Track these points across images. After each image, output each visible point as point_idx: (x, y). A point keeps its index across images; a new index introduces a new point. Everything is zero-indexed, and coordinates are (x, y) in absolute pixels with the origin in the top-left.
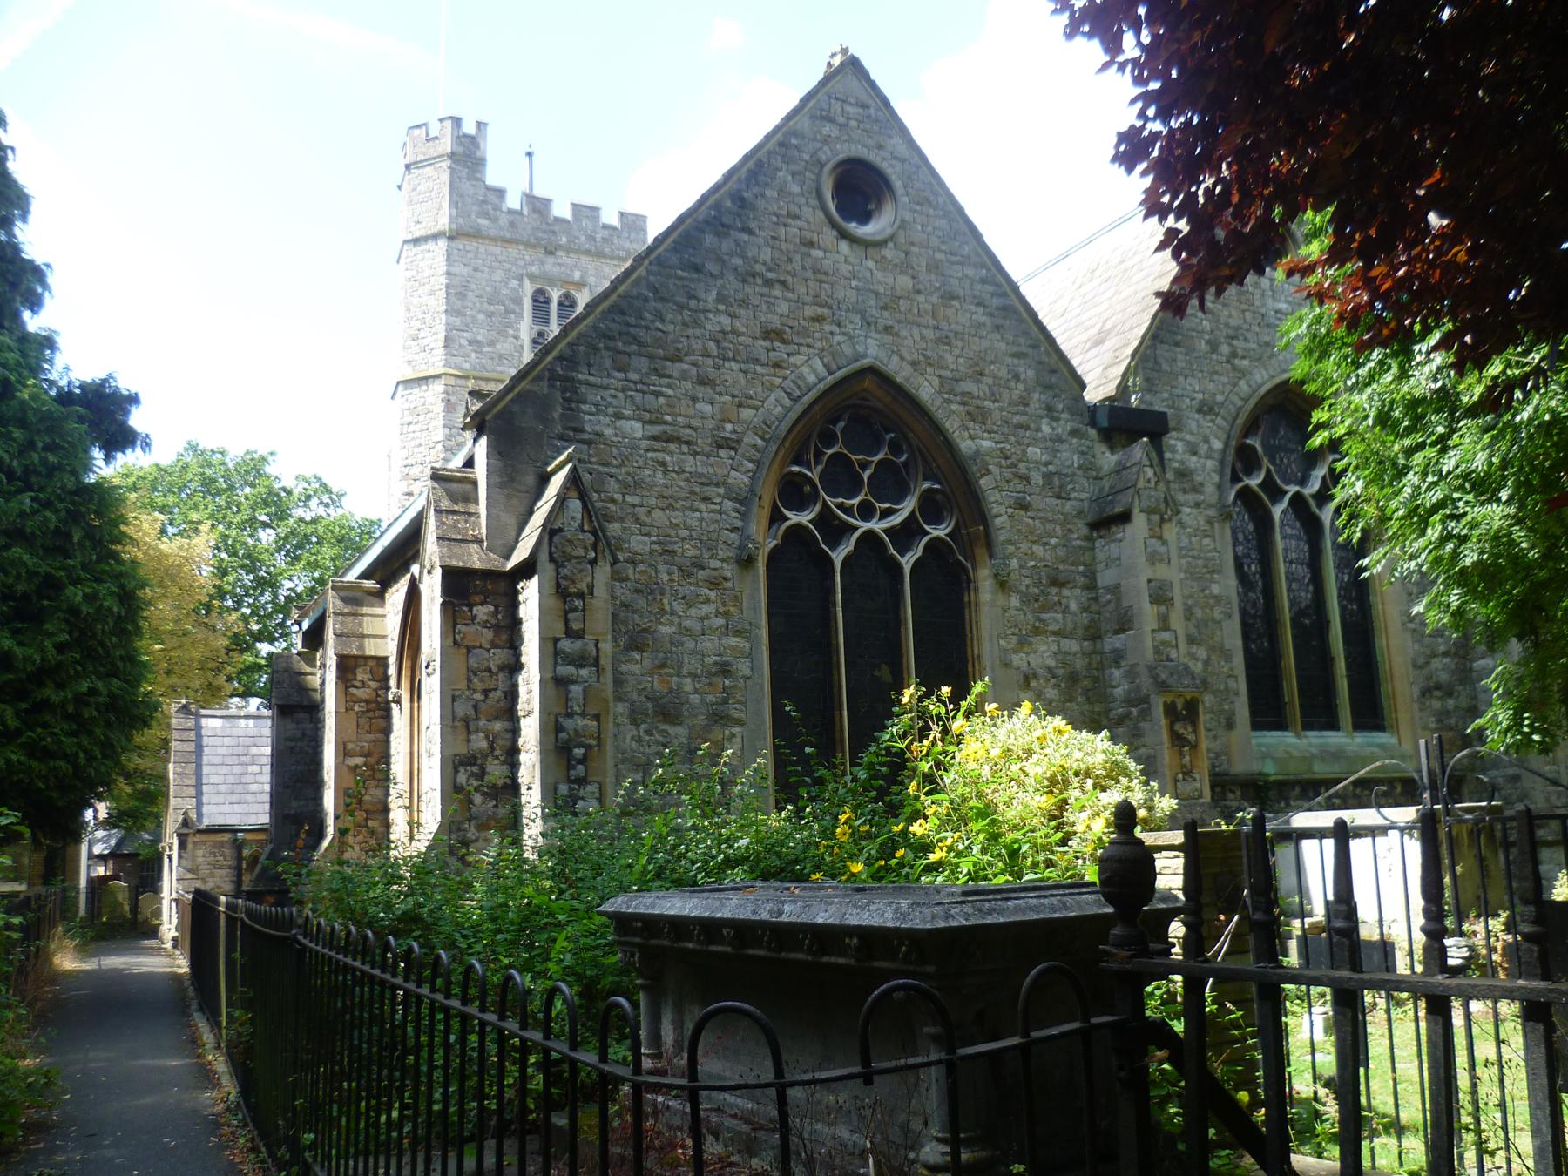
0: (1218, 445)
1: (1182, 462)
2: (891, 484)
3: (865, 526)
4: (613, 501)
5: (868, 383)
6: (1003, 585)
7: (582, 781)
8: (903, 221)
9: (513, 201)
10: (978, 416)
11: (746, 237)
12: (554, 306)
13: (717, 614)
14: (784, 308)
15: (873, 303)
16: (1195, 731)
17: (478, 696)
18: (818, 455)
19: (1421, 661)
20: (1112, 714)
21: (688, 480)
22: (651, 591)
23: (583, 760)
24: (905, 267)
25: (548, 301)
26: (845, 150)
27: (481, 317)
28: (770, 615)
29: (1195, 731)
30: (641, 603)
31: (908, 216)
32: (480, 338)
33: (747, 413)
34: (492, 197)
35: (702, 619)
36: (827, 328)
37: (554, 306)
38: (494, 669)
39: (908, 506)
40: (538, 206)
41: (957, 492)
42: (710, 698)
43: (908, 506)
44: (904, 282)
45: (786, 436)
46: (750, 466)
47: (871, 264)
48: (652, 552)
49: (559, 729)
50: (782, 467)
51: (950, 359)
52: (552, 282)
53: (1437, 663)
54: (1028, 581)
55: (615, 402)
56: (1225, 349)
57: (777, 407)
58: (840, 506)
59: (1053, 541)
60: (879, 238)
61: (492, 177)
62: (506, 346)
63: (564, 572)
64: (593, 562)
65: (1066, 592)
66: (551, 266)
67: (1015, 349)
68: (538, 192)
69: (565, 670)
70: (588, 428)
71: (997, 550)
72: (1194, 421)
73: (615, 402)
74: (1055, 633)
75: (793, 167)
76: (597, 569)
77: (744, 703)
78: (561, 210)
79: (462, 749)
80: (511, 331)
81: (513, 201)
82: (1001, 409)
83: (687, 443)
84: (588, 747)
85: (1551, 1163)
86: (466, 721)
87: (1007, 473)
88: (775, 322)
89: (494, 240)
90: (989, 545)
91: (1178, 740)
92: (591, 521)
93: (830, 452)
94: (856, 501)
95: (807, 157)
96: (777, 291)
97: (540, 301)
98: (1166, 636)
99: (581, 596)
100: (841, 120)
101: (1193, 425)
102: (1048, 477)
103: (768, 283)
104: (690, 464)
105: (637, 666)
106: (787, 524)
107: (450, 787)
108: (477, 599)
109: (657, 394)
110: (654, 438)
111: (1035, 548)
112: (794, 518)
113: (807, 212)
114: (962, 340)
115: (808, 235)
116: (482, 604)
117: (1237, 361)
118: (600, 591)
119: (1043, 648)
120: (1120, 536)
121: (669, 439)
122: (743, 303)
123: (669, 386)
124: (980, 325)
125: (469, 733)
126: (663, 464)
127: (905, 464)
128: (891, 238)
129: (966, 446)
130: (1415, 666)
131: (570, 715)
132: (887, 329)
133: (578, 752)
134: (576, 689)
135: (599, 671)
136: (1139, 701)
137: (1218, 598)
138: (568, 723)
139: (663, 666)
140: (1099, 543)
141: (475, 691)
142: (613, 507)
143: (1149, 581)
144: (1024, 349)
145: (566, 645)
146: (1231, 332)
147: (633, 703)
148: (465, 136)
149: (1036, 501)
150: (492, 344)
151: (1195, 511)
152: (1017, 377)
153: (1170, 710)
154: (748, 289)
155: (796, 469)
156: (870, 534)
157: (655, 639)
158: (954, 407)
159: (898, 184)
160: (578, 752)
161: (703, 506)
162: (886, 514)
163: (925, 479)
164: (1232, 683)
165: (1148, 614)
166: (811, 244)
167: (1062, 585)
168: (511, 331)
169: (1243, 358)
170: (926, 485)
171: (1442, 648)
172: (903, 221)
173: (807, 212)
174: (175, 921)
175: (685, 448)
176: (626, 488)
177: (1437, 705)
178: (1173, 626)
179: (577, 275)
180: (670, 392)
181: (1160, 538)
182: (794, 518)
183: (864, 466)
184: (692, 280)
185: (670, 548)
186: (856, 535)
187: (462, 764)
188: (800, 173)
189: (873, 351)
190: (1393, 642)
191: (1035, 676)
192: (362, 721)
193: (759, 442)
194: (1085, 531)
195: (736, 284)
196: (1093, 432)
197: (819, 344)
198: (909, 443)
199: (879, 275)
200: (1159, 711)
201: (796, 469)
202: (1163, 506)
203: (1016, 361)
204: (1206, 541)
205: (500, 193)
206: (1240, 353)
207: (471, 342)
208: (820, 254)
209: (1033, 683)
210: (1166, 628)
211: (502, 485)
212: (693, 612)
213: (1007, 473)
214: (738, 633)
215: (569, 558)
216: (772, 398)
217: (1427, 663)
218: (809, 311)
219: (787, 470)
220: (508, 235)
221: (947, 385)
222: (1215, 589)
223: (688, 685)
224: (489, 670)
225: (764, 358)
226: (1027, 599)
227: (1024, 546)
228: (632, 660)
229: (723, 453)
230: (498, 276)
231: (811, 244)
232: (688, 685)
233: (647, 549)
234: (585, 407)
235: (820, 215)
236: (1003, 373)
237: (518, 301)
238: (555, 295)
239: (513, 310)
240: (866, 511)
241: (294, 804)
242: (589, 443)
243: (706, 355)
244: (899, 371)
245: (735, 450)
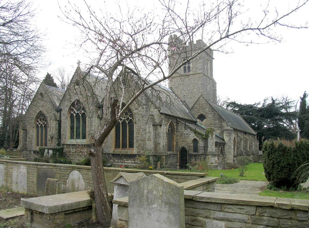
222: (66, 125)
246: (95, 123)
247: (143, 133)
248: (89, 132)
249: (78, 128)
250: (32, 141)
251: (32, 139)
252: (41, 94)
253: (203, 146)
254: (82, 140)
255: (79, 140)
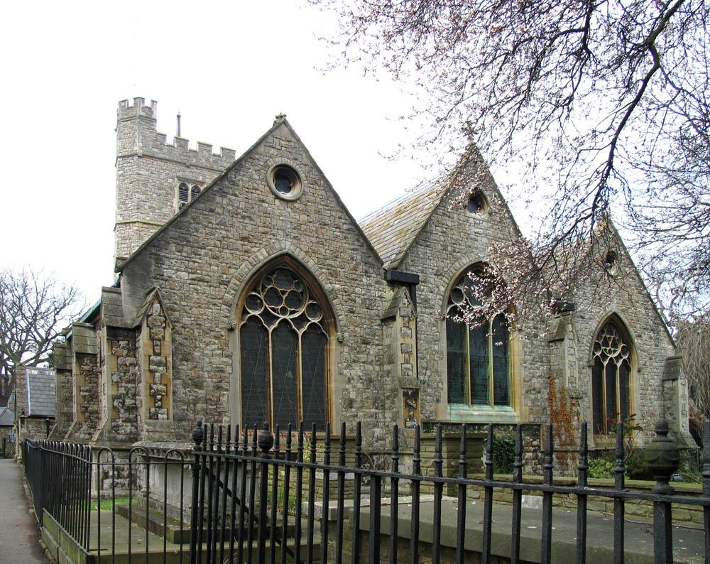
0: (443, 289)
1: (426, 296)
2: (295, 300)
3: (282, 317)
4: (175, 303)
5: (287, 259)
6: (340, 342)
7: (160, 407)
8: (304, 191)
9: (170, 140)
10: (334, 274)
11: (234, 198)
12: (190, 192)
13: (218, 349)
14: (250, 227)
15: (289, 226)
16: (416, 403)
17: (122, 374)
18: (264, 288)
19: (527, 379)
20: (386, 395)
21: (207, 297)
22: (192, 339)
23: (160, 400)
24: (305, 212)
25: (187, 190)
26: (279, 161)
27: (155, 195)
28: (242, 349)
29: (416, 403)
30: (187, 343)
31: (307, 190)
32: (154, 205)
33: (232, 271)
34: (159, 137)
35: (212, 350)
36: (269, 236)
37: (190, 192)
38: (128, 364)
39: (302, 310)
40: (182, 142)
41: (322, 304)
42: (215, 380)
43: (302, 310)
44: (304, 218)
45: (249, 281)
46: (234, 292)
47: (289, 210)
48: (192, 324)
49: (151, 388)
50: (248, 292)
51: (323, 250)
52: (189, 181)
53: (534, 380)
54: (352, 342)
55: (177, 265)
56: (450, 249)
57: (247, 269)
58: (273, 309)
59: (365, 326)
60: (292, 199)
61: (160, 128)
62: (167, 210)
63: (152, 331)
64: (165, 328)
65: (368, 347)
66: (188, 174)
67: (353, 247)
68: (183, 136)
69: (153, 367)
70: (165, 274)
71: (339, 329)
72: (432, 279)
73: (177, 265)
74: (363, 363)
75: (257, 168)
76: (166, 331)
77: (229, 383)
78: (193, 146)
79: (115, 393)
80: (169, 203)
81: (170, 140)
82: (344, 272)
83: (207, 282)
84: (162, 396)
85: (118, 448)
86: (117, 382)
87: (345, 298)
88: (245, 234)
89: (161, 159)
90: (336, 327)
91: (407, 406)
92: (164, 313)
93: (269, 287)
94: (280, 307)
95: (262, 164)
96: (247, 221)
97: (183, 189)
98: (408, 366)
99: (160, 340)
100: (279, 147)
101: (432, 281)
102: (364, 301)
103: (243, 217)
104: (208, 290)
105: (185, 367)
106: (249, 315)
107: (111, 406)
108: (122, 338)
109: (194, 262)
110: (192, 279)
111: (356, 328)
112: (252, 313)
113: (261, 187)
114: (329, 243)
115: (261, 197)
116: (123, 340)
117: (455, 254)
118: (168, 338)
119: (357, 368)
120: (391, 326)
121: (200, 280)
122: (232, 225)
123: (200, 259)
124: (337, 236)
125: (118, 387)
126: (197, 290)
127: (302, 293)
128: (299, 199)
129: (327, 287)
130: (524, 381)
131: (155, 384)
132: (295, 238)
133: (159, 397)
134: (157, 375)
135: (167, 368)
136: (394, 391)
137: (437, 352)
138: (154, 387)
139: (195, 367)
140: (385, 328)
141: (121, 372)
142: (175, 306)
143: (402, 344)
144: (356, 247)
145: (153, 358)
146: (453, 241)
147: (183, 380)
148: (146, 107)
149: (357, 310)
150: (160, 209)
151: (430, 316)
152: (353, 259)
153: (405, 394)
154: (234, 220)
155: (254, 293)
156: (285, 320)
157: (192, 357)
158: (324, 270)
159: (302, 176)
160: (159, 397)
161: (213, 307)
162: (292, 313)
163: (310, 299)
164: (440, 385)
165: (400, 357)
166: (263, 201)
167: (368, 344)
168: (169, 203)
169: (458, 252)
170: (310, 302)
171: (538, 374)
172: (304, 191)
173: (261, 187)
174: (21, 452)
175: (206, 284)
176: (181, 299)
177: (533, 397)
178: (411, 362)
179: (201, 178)
180: (200, 261)
181: (408, 327)
182: (252, 313)
183: (283, 293)
184: (210, 216)
185: (199, 322)
186: (278, 321)
187: (115, 398)
188: (259, 170)
189: (288, 246)
190: (516, 371)
191: (353, 379)
192: (87, 378)
193: (238, 283)
194: (379, 322)
195: (229, 218)
196: (385, 282)
197: (264, 243)
198: (303, 284)
199: (292, 214)
200: (401, 395)
201: (254, 293)
202: (410, 315)
203: (353, 252)
204: (434, 328)
205: (164, 136)
206: (457, 250)
207: (150, 208)
208: (267, 205)
209: (352, 382)
210: (408, 363)
211: (130, 296)
212: (208, 347)
213: (345, 298)
214: (227, 356)
215: (155, 326)
216: (243, 265)
217: (530, 380)
218: (261, 229)
219: (250, 294)
220: (167, 157)
221: (321, 263)
222: (436, 348)
223: (206, 375)
224: (126, 365)
225: (240, 248)
226: (352, 349)
227: (352, 328)
228: (183, 364)
229: (222, 286)
230: (163, 176)
231: (263, 201)
232: (206, 375)
233: (190, 323)
234: (164, 266)
235: (267, 188)
236: (347, 256)
237: (172, 188)
238: (190, 187)
239: (169, 194)
240: (283, 311)
241: (66, 409)
242: (166, 280)
243: (215, 246)
244: (300, 255)
245: (227, 285)
246: (571, 358)
247: (652, 397)
248: (529, 383)
249: (479, 364)
250: (218, 402)
251: (218, 388)
252: (611, 258)
253: (325, 452)
254: (497, 408)
255: (485, 407)
